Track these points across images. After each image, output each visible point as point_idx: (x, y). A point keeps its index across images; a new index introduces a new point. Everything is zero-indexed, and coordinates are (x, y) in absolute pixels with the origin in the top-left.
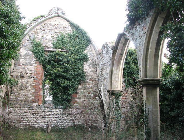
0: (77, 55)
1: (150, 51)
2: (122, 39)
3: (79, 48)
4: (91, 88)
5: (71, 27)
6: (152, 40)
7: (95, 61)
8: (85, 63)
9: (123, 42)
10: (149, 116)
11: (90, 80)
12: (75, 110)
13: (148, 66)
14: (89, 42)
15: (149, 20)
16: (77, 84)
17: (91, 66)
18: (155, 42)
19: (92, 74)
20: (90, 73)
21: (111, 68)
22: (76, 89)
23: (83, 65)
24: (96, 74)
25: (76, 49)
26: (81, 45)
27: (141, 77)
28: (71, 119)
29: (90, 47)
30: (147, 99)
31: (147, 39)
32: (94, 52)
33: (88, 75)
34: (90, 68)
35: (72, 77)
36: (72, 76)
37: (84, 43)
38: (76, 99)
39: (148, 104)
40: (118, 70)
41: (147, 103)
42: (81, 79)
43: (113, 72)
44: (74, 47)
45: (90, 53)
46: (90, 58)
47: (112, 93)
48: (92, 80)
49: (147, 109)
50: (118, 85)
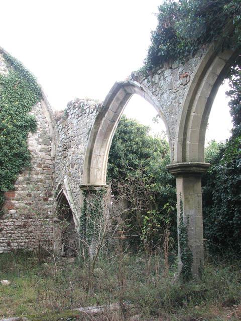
0: (17, 117)
1: (194, 116)
2: (122, 91)
3: (22, 105)
4: (41, 181)
5: (5, 65)
6: (200, 97)
7: (48, 132)
8: (30, 134)
9: (121, 99)
10: (189, 228)
11: (39, 165)
12: (11, 222)
13: (188, 142)
14: (38, 95)
15: (196, 63)
16: (16, 173)
17: (40, 140)
18: (204, 101)
19: (43, 155)
20: (40, 153)
21: (90, 144)
22: (13, 182)
23: (27, 138)
24: (50, 155)
25: (14, 107)
26: (25, 101)
27: (176, 160)
28: (3, 240)
29: (40, 106)
30: (186, 199)
31: (191, 95)
32: (47, 115)
33: (36, 156)
34: (39, 143)
35: (7, 159)
36: (7, 157)
37: (30, 96)
38: (13, 202)
39: (187, 207)
40: (103, 149)
41: (185, 206)
42: (23, 164)
43: (93, 153)
44: (11, 102)
45: (40, 116)
46: (39, 126)
47: (89, 191)
48: (43, 166)
49: (185, 215)
50: (101, 176)
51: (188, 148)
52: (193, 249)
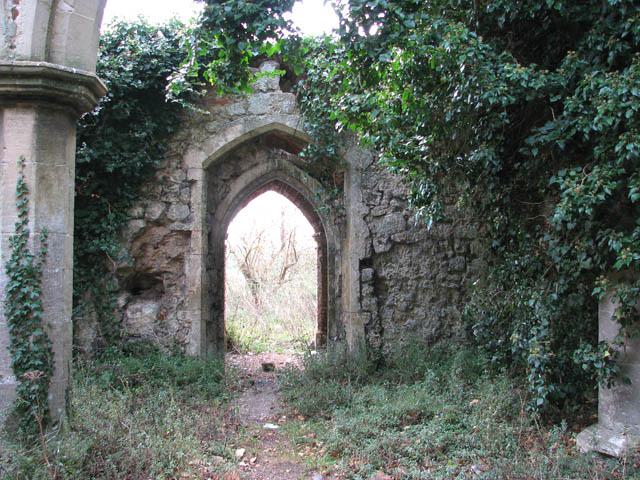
10: (46, 271)
30: (42, 178)
39: (44, 205)
41: (38, 200)
49: (37, 230)
51: (63, 26)
52: (54, 333)
